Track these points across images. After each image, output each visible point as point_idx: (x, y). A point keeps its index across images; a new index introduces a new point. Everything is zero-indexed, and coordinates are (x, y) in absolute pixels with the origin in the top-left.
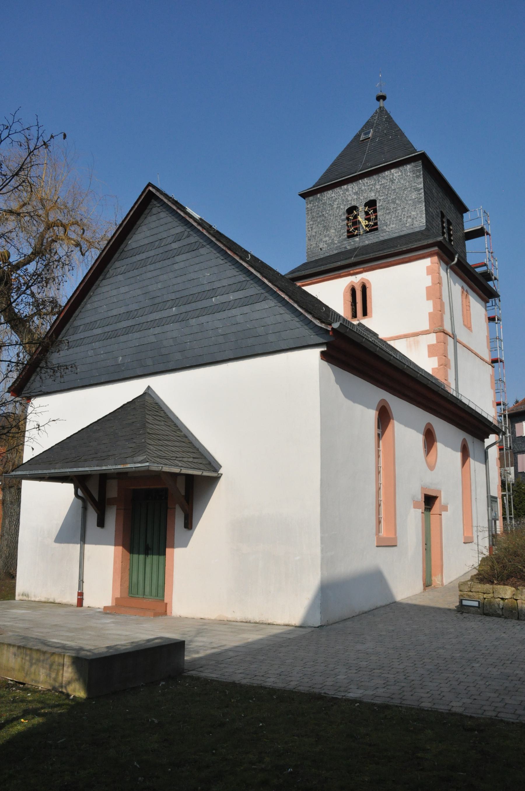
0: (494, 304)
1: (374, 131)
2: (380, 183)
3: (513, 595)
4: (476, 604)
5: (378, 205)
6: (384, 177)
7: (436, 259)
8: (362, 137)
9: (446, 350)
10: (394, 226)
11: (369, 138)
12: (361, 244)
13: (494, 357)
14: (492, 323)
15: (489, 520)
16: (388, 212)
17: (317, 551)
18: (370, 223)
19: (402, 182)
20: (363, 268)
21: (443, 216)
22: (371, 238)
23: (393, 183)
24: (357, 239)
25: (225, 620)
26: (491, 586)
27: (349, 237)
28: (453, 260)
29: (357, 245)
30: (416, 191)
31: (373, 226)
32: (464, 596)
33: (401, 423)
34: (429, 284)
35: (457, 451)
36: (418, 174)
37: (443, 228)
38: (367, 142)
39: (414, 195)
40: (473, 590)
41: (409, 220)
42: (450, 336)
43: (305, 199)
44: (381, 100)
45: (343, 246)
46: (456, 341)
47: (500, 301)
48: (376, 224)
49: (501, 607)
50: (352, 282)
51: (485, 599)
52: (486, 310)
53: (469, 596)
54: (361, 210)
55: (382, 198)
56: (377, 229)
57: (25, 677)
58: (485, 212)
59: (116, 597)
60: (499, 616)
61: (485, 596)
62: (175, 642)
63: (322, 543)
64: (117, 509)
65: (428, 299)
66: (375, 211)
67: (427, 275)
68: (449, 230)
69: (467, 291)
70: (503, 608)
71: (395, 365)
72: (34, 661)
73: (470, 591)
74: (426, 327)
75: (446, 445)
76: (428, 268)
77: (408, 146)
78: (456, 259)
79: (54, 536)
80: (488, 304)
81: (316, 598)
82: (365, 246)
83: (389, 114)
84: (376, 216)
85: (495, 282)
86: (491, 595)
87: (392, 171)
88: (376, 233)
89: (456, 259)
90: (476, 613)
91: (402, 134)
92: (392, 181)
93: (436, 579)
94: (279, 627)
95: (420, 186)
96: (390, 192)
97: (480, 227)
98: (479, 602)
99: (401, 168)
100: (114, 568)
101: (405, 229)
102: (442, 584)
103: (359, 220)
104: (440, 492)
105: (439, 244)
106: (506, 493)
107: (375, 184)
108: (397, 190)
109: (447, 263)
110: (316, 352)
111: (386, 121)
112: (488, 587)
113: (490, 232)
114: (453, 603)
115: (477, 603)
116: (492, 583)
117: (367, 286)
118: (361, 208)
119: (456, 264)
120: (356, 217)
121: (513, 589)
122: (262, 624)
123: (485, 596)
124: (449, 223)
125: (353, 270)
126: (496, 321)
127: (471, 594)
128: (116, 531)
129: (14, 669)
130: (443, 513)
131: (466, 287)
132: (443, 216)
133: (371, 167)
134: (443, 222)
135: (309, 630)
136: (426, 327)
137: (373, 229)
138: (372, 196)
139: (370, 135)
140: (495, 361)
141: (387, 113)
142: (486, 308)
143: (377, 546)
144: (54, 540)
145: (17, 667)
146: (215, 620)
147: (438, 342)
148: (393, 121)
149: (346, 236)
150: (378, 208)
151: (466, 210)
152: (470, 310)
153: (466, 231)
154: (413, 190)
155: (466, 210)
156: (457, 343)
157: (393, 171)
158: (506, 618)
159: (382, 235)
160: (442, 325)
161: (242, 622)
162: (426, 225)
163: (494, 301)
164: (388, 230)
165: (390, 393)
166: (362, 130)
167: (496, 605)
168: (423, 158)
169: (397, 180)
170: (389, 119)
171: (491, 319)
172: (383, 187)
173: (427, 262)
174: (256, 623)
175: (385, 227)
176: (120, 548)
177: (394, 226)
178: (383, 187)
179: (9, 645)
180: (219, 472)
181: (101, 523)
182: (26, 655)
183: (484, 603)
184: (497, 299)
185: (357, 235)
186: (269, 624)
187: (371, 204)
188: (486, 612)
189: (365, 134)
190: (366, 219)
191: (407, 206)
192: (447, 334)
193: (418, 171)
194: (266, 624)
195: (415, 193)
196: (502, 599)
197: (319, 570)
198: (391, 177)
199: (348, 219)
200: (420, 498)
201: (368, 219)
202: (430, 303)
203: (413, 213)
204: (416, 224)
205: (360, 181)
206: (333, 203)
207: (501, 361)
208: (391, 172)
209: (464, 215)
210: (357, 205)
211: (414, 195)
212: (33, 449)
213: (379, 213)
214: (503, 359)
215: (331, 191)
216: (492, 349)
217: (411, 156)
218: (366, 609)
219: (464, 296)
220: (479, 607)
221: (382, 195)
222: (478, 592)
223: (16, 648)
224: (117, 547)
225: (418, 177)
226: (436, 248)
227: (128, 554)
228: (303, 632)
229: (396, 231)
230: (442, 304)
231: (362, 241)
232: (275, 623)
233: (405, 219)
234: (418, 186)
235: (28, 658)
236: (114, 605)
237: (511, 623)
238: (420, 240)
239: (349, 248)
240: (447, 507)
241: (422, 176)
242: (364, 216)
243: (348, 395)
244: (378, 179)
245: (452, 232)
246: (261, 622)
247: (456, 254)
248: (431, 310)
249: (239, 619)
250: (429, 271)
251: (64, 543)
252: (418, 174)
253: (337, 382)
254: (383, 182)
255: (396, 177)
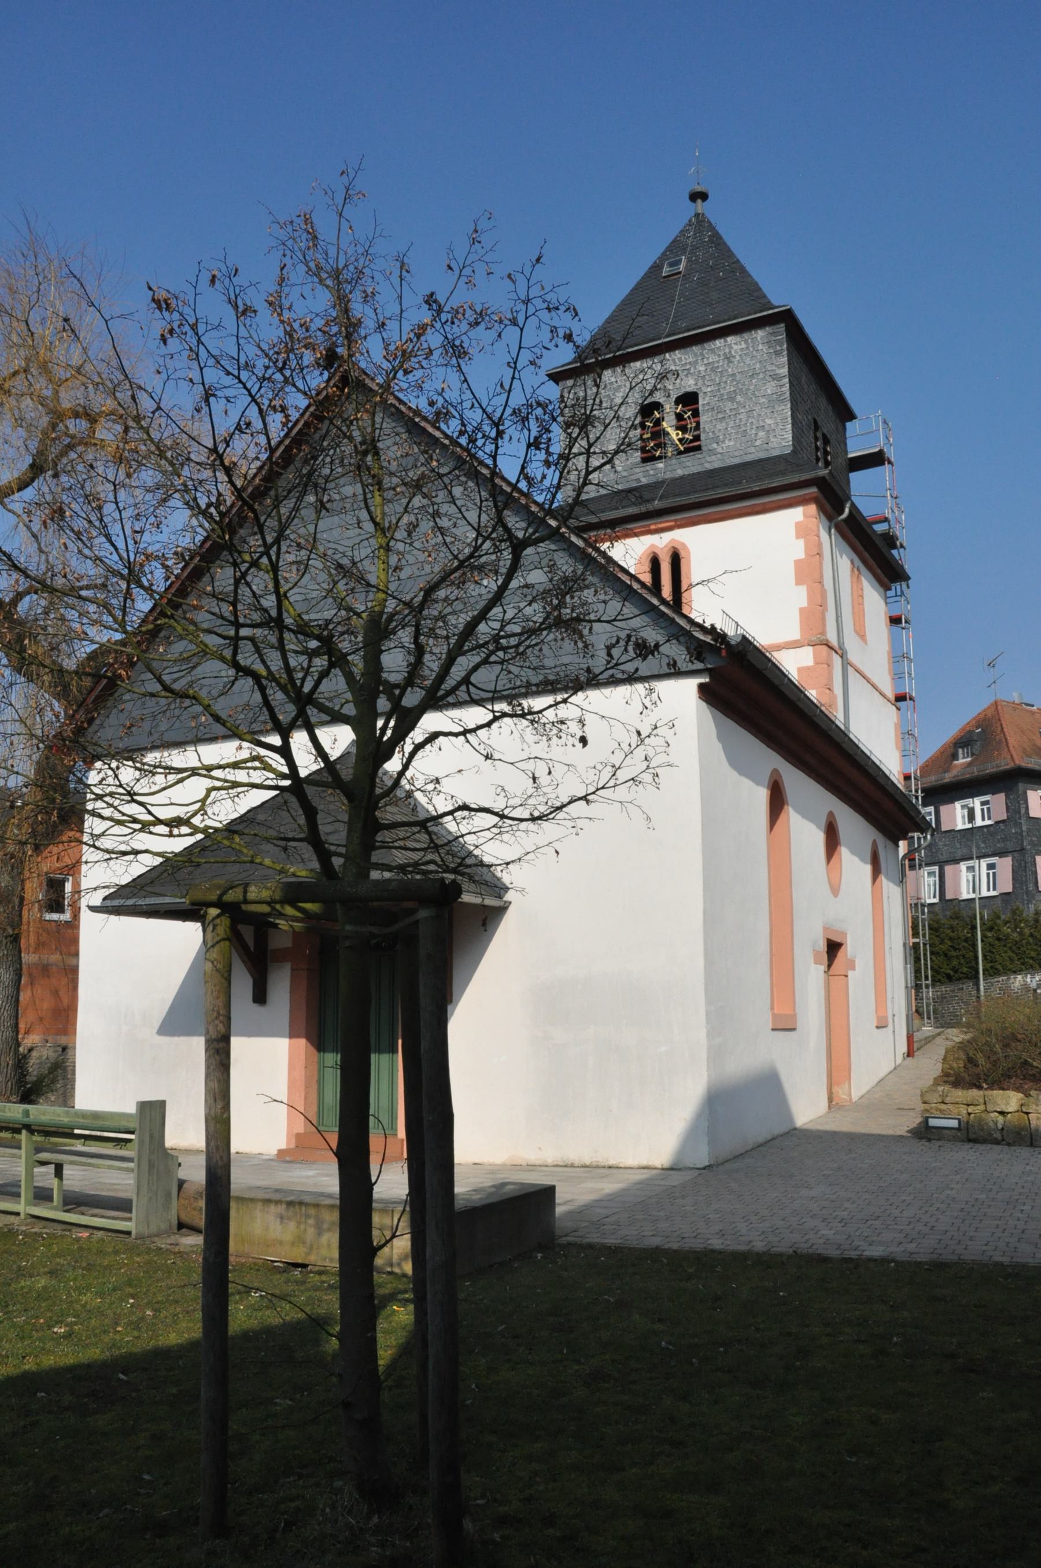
0: (899, 593)
1: (689, 260)
2: (706, 361)
3: (1022, 1105)
4: (954, 1123)
5: (701, 402)
6: (712, 351)
7: (812, 508)
8: (666, 271)
9: (830, 678)
10: (732, 443)
11: (680, 273)
12: (669, 475)
13: (901, 691)
14: (896, 629)
15: (907, 987)
16: (720, 416)
17: (701, 1034)
18: (687, 436)
19: (748, 361)
20: (675, 521)
21: (817, 427)
22: (688, 464)
23: (730, 362)
24: (661, 465)
25: (524, 1163)
26: (981, 1093)
27: (645, 460)
28: (842, 512)
29: (661, 477)
30: (774, 379)
31: (692, 441)
32: (933, 1111)
33: (797, 811)
34: (801, 554)
35: (866, 863)
36: (778, 348)
37: (817, 449)
38: (677, 280)
39: (770, 388)
40: (948, 1100)
41: (761, 434)
42: (836, 652)
43: (557, 384)
44: (699, 201)
45: (633, 477)
46: (846, 664)
47: (908, 587)
48: (697, 438)
49: (1000, 1126)
50: (652, 545)
51: (969, 1114)
52: (886, 603)
53: (941, 1111)
54: (668, 410)
55: (709, 389)
56: (698, 448)
57: (308, 1254)
58: (885, 422)
59: (296, 1132)
60: (997, 1142)
61: (970, 1109)
62: (537, 1188)
63: (708, 1023)
64: (292, 970)
65: (799, 582)
66: (696, 413)
67: (797, 537)
68: (826, 453)
69: (858, 570)
70: (1003, 1129)
71: (806, 710)
72: (325, 1226)
73: (943, 1102)
74: (795, 634)
75: (853, 852)
76: (797, 524)
77: (754, 293)
78: (847, 511)
79: (157, 1024)
80: (890, 593)
81: (699, 1116)
82: (677, 479)
83: (714, 228)
84: (698, 423)
85: (902, 550)
86: (982, 1107)
87: (729, 339)
88: (698, 455)
89: (847, 511)
90: (955, 1139)
91: (743, 270)
92: (728, 358)
93: (840, 1091)
94: (632, 1171)
95: (782, 371)
96: (724, 379)
97: (876, 450)
98: (959, 1120)
99: (746, 335)
100: (290, 1080)
101: (753, 450)
102: (851, 1099)
103: (664, 430)
104: (845, 935)
105: (820, 483)
106: (920, 940)
107: (696, 363)
108: (738, 377)
109: (830, 518)
110: (689, 686)
111: (711, 241)
112: (974, 1094)
113: (893, 460)
114: (905, 1123)
115: (956, 1122)
116: (980, 1088)
117: (682, 554)
118: (669, 407)
119: (845, 520)
120: (658, 422)
121: (1021, 1095)
122: (598, 1167)
123: (970, 1109)
124: (826, 441)
125: (655, 524)
126: (904, 625)
127: (943, 1107)
128: (291, 1011)
129: (281, 1243)
130: (850, 973)
131: (858, 562)
132: (817, 427)
133: (689, 330)
134: (816, 439)
135: (689, 1176)
136: (795, 634)
137: (693, 447)
138: (689, 384)
139: (682, 267)
140: (900, 698)
141: (711, 227)
142: (886, 598)
143: (773, 1030)
144: (155, 1030)
145: (288, 1237)
146: (504, 1165)
147: (817, 663)
148: (725, 243)
149: (639, 459)
150: (701, 408)
151: (852, 416)
152: (862, 604)
153: (850, 455)
154: (769, 379)
155: (852, 416)
156: (849, 668)
157: (730, 339)
158: (1009, 1144)
159: (709, 459)
160: (823, 632)
161: (557, 1166)
162: (793, 444)
163: (898, 587)
164: (720, 450)
165: (784, 758)
166: (663, 257)
167: (991, 1124)
168: (788, 319)
169: (738, 357)
170: (717, 240)
171: (895, 621)
172: (712, 370)
173: (796, 514)
174: (585, 1166)
175: (715, 445)
176: (302, 1042)
177: (732, 443)
178: (712, 370)
179: (267, 1201)
180: (505, 899)
181: (260, 997)
182: (308, 1216)
183: (968, 1122)
184: (904, 585)
185: (660, 458)
186: (610, 1167)
187: (689, 400)
188: (972, 1136)
189: (671, 265)
190: (677, 428)
191: (757, 408)
192: (831, 648)
193: (779, 343)
194: (604, 1167)
195: (773, 383)
196: (1002, 1113)
197: (705, 1068)
198: (727, 351)
199: (643, 426)
200: (822, 946)
201: (683, 429)
202: (803, 590)
203: (769, 421)
204: (774, 442)
205: (667, 355)
206: (614, 394)
207: (911, 699)
208: (726, 341)
209: (848, 424)
210: (661, 401)
211: (770, 388)
212: (557, 852)
213: (703, 418)
214: (914, 695)
215: (610, 371)
216: (897, 676)
217: (765, 313)
218: (761, 1139)
219: (855, 579)
220: (959, 1129)
221: (709, 383)
222: (957, 1103)
223: (284, 1206)
224: (296, 1041)
225: (778, 353)
226: (814, 490)
227: (315, 1052)
228: (676, 1179)
229: (736, 454)
230: (823, 593)
231: (669, 468)
232: (621, 1165)
233: (754, 431)
234: (778, 372)
235: (311, 1221)
236: (293, 1146)
237: (1025, 1152)
238: (783, 473)
239: (644, 481)
240: (854, 961)
241: (785, 353)
242: (674, 422)
243: (734, 762)
244: (702, 354)
245: (829, 458)
246: (594, 1164)
247: (847, 501)
248: (804, 603)
249: (550, 1161)
250: (801, 531)
251: (179, 1035)
252: (778, 348)
253: (720, 738)
254: (711, 360)
255: (736, 352)
